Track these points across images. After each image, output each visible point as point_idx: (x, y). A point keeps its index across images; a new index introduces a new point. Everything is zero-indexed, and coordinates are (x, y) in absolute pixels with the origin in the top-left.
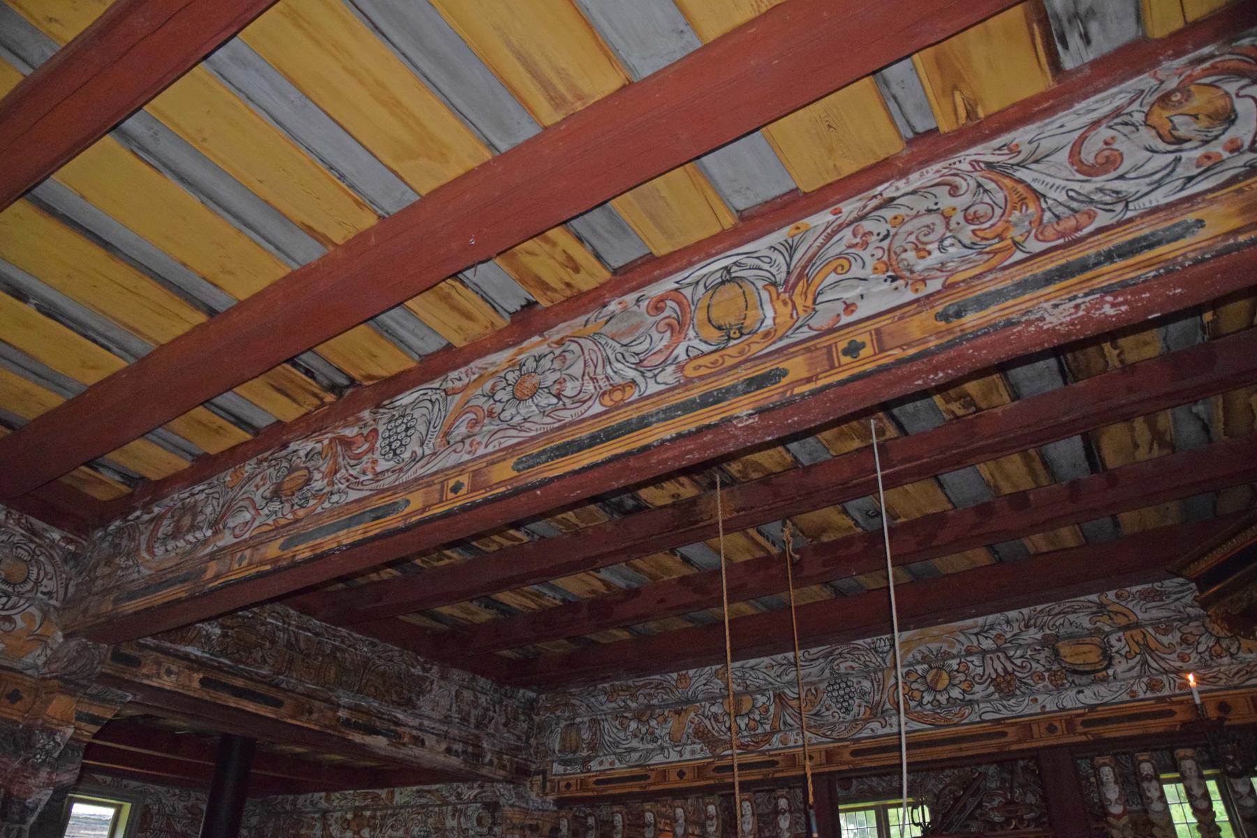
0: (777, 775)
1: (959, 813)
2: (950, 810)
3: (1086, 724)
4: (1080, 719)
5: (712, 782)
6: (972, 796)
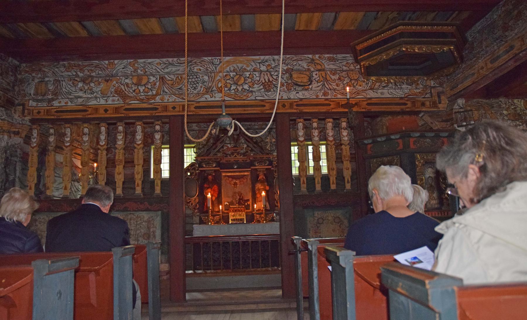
0: (157, 114)
1: (214, 149)
2: (210, 148)
3: (297, 105)
4: (295, 103)
5: (123, 115)
6: (220, 143)
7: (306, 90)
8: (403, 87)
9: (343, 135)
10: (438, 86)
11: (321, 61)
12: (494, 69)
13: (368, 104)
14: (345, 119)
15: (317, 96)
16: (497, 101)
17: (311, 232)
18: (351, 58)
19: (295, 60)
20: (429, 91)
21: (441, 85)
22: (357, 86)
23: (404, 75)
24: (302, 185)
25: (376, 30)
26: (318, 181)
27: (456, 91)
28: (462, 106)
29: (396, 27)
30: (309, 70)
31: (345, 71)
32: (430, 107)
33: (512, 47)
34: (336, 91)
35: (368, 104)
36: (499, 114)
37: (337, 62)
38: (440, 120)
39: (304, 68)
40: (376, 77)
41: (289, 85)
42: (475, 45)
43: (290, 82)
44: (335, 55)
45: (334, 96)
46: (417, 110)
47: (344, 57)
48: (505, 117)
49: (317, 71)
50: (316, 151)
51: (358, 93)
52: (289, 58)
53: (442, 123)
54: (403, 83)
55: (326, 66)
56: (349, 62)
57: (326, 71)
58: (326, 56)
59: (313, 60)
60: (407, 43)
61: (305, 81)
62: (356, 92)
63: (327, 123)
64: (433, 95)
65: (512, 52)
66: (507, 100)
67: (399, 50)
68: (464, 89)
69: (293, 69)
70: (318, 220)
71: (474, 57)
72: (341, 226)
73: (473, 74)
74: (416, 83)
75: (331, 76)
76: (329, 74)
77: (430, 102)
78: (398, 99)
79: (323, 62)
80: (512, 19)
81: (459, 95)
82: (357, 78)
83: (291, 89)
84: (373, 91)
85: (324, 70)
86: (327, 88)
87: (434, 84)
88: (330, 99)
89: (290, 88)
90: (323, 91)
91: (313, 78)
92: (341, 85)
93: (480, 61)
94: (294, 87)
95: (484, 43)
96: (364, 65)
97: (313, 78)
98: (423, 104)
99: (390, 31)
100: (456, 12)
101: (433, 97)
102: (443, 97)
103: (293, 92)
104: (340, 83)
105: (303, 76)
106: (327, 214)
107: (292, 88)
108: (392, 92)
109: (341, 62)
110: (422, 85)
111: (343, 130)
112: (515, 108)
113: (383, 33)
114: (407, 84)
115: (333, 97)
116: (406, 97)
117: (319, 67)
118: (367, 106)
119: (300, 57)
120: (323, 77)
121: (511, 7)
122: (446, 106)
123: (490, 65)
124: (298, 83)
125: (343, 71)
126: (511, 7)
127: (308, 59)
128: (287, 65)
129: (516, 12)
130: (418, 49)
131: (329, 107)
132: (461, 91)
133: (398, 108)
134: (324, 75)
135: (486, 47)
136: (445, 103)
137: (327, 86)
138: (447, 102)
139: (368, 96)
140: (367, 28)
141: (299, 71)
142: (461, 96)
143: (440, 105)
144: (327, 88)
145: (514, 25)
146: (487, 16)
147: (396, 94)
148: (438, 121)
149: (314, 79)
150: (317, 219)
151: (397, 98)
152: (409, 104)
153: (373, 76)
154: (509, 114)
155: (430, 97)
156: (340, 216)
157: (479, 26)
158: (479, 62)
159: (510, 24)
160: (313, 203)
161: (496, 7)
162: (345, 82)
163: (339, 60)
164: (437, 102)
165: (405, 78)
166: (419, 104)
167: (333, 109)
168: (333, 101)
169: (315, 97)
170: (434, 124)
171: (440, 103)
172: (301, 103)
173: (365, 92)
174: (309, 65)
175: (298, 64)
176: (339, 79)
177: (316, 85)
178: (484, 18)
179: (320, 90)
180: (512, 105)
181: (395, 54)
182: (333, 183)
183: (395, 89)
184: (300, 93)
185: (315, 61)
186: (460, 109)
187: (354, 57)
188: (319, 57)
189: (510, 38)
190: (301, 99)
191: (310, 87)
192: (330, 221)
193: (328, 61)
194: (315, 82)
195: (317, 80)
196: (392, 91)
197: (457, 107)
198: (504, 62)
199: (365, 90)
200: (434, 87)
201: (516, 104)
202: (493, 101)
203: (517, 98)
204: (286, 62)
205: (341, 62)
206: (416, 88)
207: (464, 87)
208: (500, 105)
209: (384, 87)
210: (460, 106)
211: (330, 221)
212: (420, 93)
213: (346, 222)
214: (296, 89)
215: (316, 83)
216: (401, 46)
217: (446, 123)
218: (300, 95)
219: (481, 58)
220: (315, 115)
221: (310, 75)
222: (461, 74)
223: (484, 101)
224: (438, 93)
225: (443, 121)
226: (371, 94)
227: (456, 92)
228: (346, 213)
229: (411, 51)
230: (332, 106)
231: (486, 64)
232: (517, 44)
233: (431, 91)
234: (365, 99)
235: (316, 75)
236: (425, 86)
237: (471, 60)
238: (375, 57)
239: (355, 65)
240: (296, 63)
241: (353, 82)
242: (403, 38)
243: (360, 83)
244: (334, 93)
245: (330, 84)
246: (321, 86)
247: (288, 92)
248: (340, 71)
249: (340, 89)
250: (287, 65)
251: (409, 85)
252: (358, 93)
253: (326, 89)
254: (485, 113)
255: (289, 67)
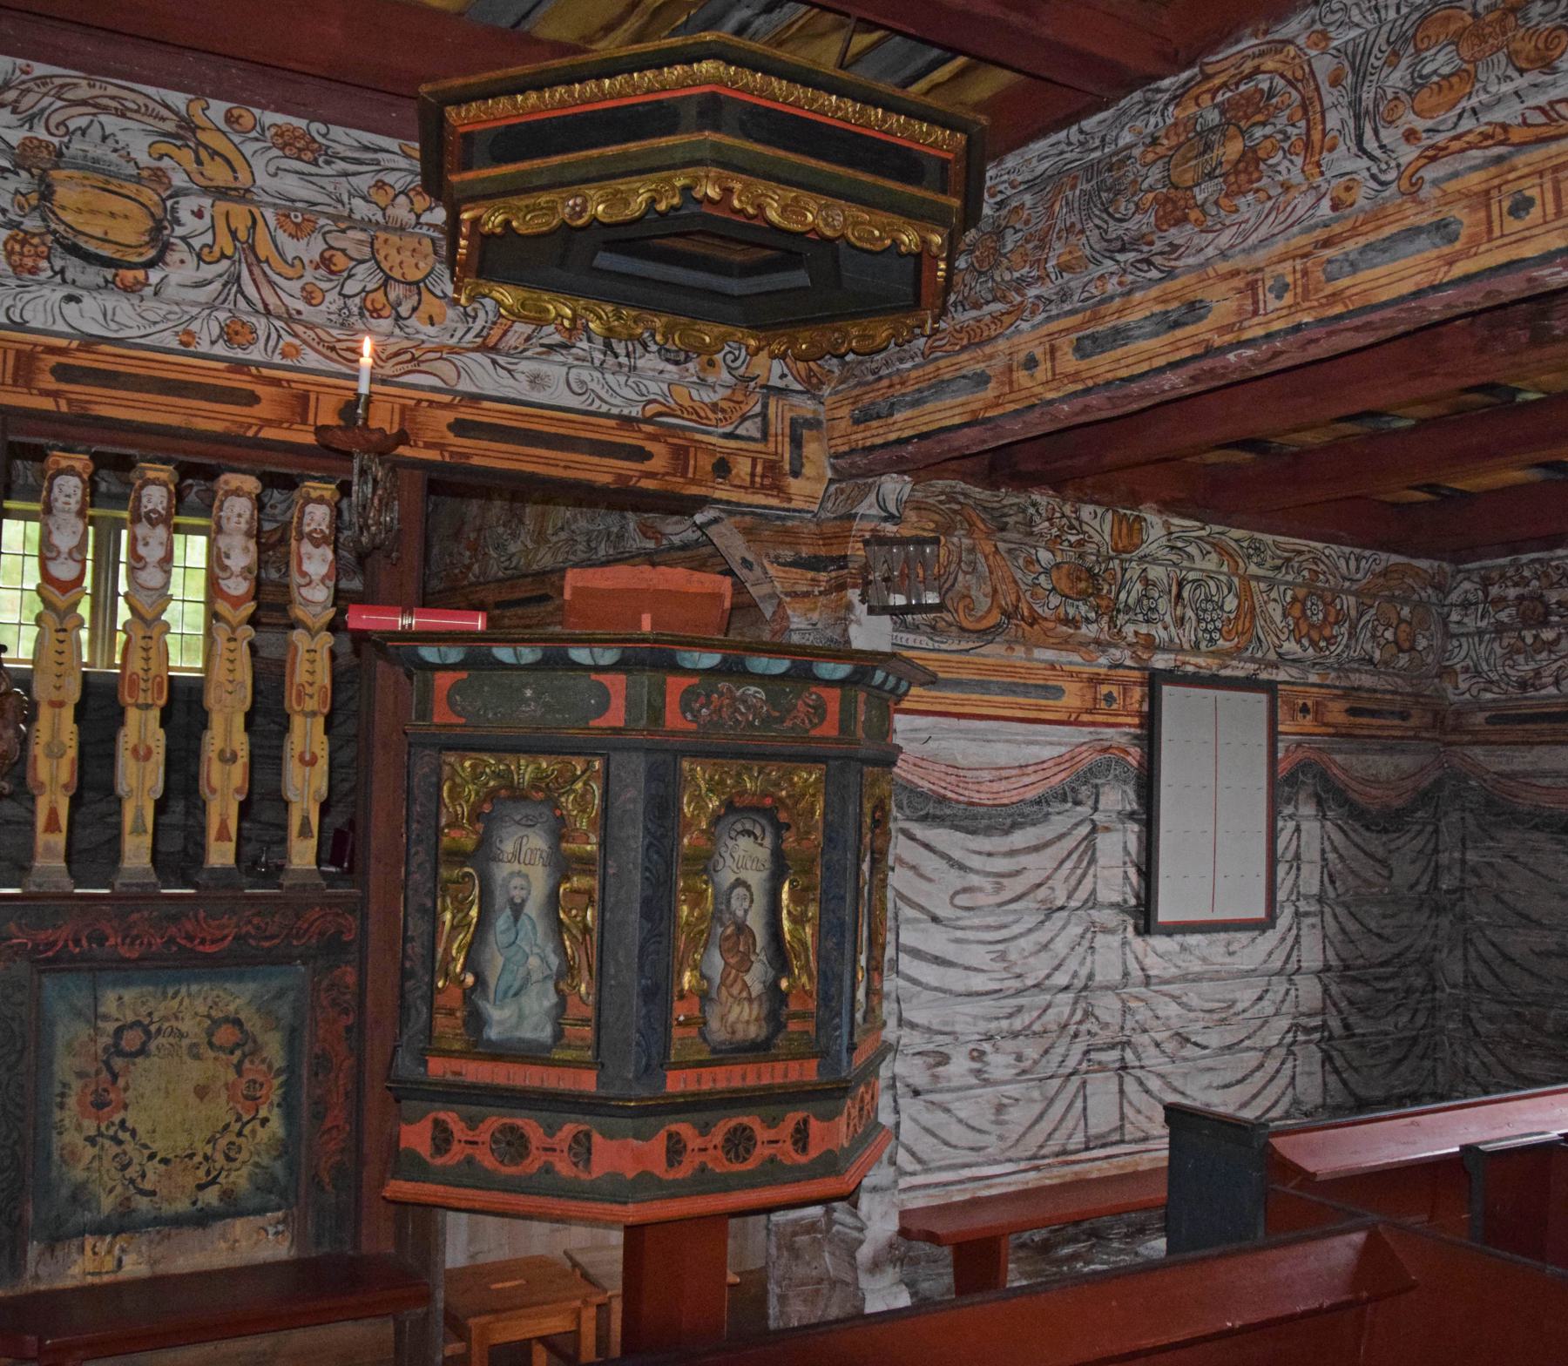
3: (63, 373)
4: (54, 360)
7: (128, 289)
8: (640, 363)
9: (304, 574)
10: (799, 387)
11: (237, 139)
12: (1090, 383)
13: (460, 427)
14: (329, 490)
15: (188, 338)
16: (1021, 499)
17: (72, 1101)
18: (403, 163)
19: (84, 103)
20: (758, 409)
21: (812, 387)
22: (413, 321)
23: (657, 310)
24: (42, 838)
25: (561, 49)
26: (139, 816)
27: (876, 433)
28: (893, 510)
29: (689, 61)
30: (158, 176)
31: (366, 224)
32: (752, 487)
33: (1194, 310)
34: (299, 329)
35: (460, 427)
36: (1021, 561)
37: (327, 170)
38: (788, 554)
39: (129, 158)
40: (522, 294)
41: (23, 243)
42: (1010, 246)
43: (32, 224)
44: (316, 128)
45: (284, 355)
46: (694, 490)
47: (366, 148)
48: (1042, 578)
49: (206, 190)
50: (146, 650)
51: (413, 358)
52: (43, 80)
53: (795, 573)
54: (645, 346)
55: (262, 179)
56: (389, 178)
57: (259, 204)
58: (271, 118)
59: (188, 126)
60: (726, 162)
61: (132, 239)
62: (404, 351)
63: (228, 494)
64: (772, 430)
65: (1189, 330)
66: (1056, 502)
67: (686, 189)
68: (922, 436)
69: (60, 154)
70: (119, 1032)
71: (995, 299)
72: (247, 1065)
73: (981, 380)
74: (705, 358)
75: (282, 237)
76: (272, 222)
77: (754, 461)
78: (612, 423)
79: (248, 149)
80: (1210, 176)
81: (893, 457)
82: (419, 275)
83: (34, 271)
84: (494, 362)
85: (243, 195)
86: (249, 301)
87: (783, 376)
88: (258, 365)
89: (29, 262)
90: (222, 316)
91: (179, 231)
92: (330, 297)
93: (1024, 326)
94: (58, 264)
95: (1059, 247)
96: (475, 222)
97: (179, 231)
98: (722, 468)
99: (649, 74)
100: (961, 61)
101: (772, 439)
102: (811, 449)
103: (46, 291)
104: (325, 285)
105: (118, 204)
106: (175, 1003)
107: (44, 264)
108: (583, 383)
109: (346, 174)
110: (730, 369)
111: (306, 547)
112: (1080, 543)
113: (610, 76)
114: (663, 352)
115: (277, 359)
116: (648, 420)
117: (218, 174)
118: (451, 438)
119: (111, 91)
120: (234, 234)
121: (1213, 117)
122: (819, 489)
123: (1069, 362)
124: (81, 242)
125: (349, 222)
126: (1213, 117)
127: (165, 113)
128: (30, 120)
129: (1234, 149)
130: (784, 210)
131: (246, 410)
132: (908, 440)
133: (601, 471)
134: (241, 225)
135: (1062, 268)
136: (819, 479)
137: (250, 290)
138: (829, 474)
139: (465, 386)
140: (518, 23)
141: (103, 177)
142: (899, 466)
143: (794, 485)
144: (249, 301)
145: (1216, 203)
146: (1089, 124)
147: (603, 394)
148: (776, 560)
149: (184, 239)
150: (110, 1027)
151: (607, 415)
152: (658, 463)
153: (504, 281)
154: (1058, 566)
155: (758, 435)
156: (242, 1016)
157: (1041, 159)
158: (1018, 331)
159: (1200, 198)
160: (102, 940)
161: (1137, 96)
162: (352, 287)
163: (336, 156)
164: (787, 467)
165: (658, 324)
166: (706, 463)
167: (268, 423)
168: (276, 382)
169: (175, 344)
170: (758, 571)
171: (796, 474)
172: (84, 360)
173: (454, 357)
174: (164, 148)
175: (95, 131)
176: (325, 262)
177: (190, 272)
178: (1075, 128)
179: (212, 306)
180: (1072, 527)
181: (662, 207)
182: (223, 835)
183: (601, 368)
184: (88, 302)
185: (201, 136)
186: (885, 519)
187: (424, 160)
188: (229, 118)
189: (1191, 261)
190: (89, 342)
191: (155, 276)
192: (185, 1042)
193: (276, 152)
194: (186, 256)
195: (197, 243)
196: (585, 375)
197: (875, 511)
198: (1145, 367)
199: (453, 350)
200: (783, 392)
201: (1086, 528)
202: (1009, 498)
203: (1092, 502)
204: (24, 105)
205: (346, 174)
206: (702, 382)
207: (925, 429)
208: (1030, 523)
209: (551, 348)
210: (885, 510)
211: (185, 1042)
212: (714, 407)
213: (274, 1048)
214: (69, 275)
215: (192, 261)
216: (701, 172)
217: (810, 575)
218: (88, 316)
219: (1033, 313)
220: (163, 442)
221: (158, 212)
222: (918, 360)
223: (977, 492)
224: (793, 422)
225: (798, 563)
226: (481, 375)
227: (879, 441)
228: (280, 994)
229: (741, 211)
230: (261, 411)
231: (1053, 351)
232: (1223, 304)
233: (765, 406)
234: (447, 399)
235: (199, 214)
236: (745, 380)
237: (977, 306)
238: (544, 199)
239: (422, 202)
240: (83, 122)
241: (395, 292)
242: (717, 128)
243: (430, 305)
244: (287, 338)
245: (272, 283)
246: (217, 285)
247: (13, 282)
248: (335, 218)
249: (319, 319)
250: (30, 120)
251: (668, 360)
252: (413, 358)
253: (242, 304)
254: (972, 550)
255: (42, 134)
